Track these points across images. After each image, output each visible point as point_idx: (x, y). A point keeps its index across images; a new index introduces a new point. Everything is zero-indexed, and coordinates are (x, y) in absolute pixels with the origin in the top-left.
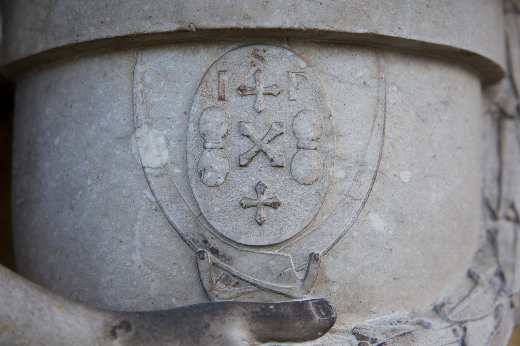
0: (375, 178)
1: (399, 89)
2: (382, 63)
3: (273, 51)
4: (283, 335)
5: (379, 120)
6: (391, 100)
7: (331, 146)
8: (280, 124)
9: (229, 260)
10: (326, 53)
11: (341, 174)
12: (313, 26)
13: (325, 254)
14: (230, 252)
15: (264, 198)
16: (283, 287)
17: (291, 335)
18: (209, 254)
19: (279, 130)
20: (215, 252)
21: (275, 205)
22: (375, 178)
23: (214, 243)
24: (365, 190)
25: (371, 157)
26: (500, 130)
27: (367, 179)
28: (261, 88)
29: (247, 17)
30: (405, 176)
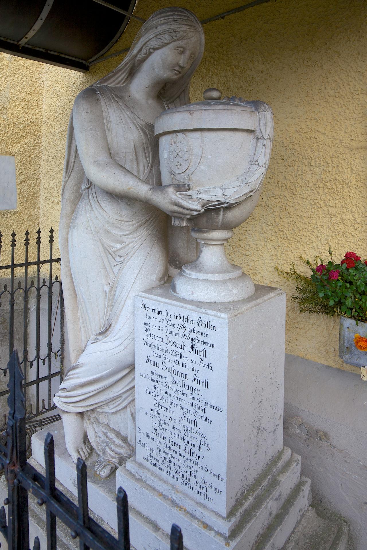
0: (201, 158)
1: (207, 138)
2: (202, 133)
3: (179, 134)
4: (180, 190)
5: (202, 146)
6: (205, 141)
7: (190, 152)
8: (181, 149)
9: (175, 176)
10: (190, 133)
11: (194, 158)
12: (183, 129)
13: (191, 174)
14: (176, 175)
15: (179, 164)
16: (184, 181)
17: (182, 191)
18: (172, 175)
19: (180, 150)
20: (173, 174)
21: (181, 165)
22: (201, 158)
23: (173, 173)
24: (199, 161)
25: (200, 154)
26: (257, 142)
27: (199, 159)
28: (177, 142)
29: (172, 129)
30: (210, 157)
